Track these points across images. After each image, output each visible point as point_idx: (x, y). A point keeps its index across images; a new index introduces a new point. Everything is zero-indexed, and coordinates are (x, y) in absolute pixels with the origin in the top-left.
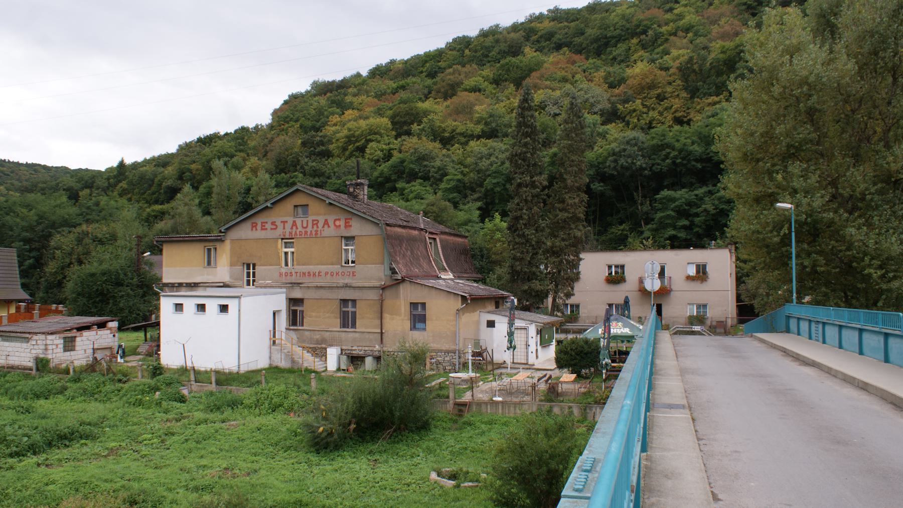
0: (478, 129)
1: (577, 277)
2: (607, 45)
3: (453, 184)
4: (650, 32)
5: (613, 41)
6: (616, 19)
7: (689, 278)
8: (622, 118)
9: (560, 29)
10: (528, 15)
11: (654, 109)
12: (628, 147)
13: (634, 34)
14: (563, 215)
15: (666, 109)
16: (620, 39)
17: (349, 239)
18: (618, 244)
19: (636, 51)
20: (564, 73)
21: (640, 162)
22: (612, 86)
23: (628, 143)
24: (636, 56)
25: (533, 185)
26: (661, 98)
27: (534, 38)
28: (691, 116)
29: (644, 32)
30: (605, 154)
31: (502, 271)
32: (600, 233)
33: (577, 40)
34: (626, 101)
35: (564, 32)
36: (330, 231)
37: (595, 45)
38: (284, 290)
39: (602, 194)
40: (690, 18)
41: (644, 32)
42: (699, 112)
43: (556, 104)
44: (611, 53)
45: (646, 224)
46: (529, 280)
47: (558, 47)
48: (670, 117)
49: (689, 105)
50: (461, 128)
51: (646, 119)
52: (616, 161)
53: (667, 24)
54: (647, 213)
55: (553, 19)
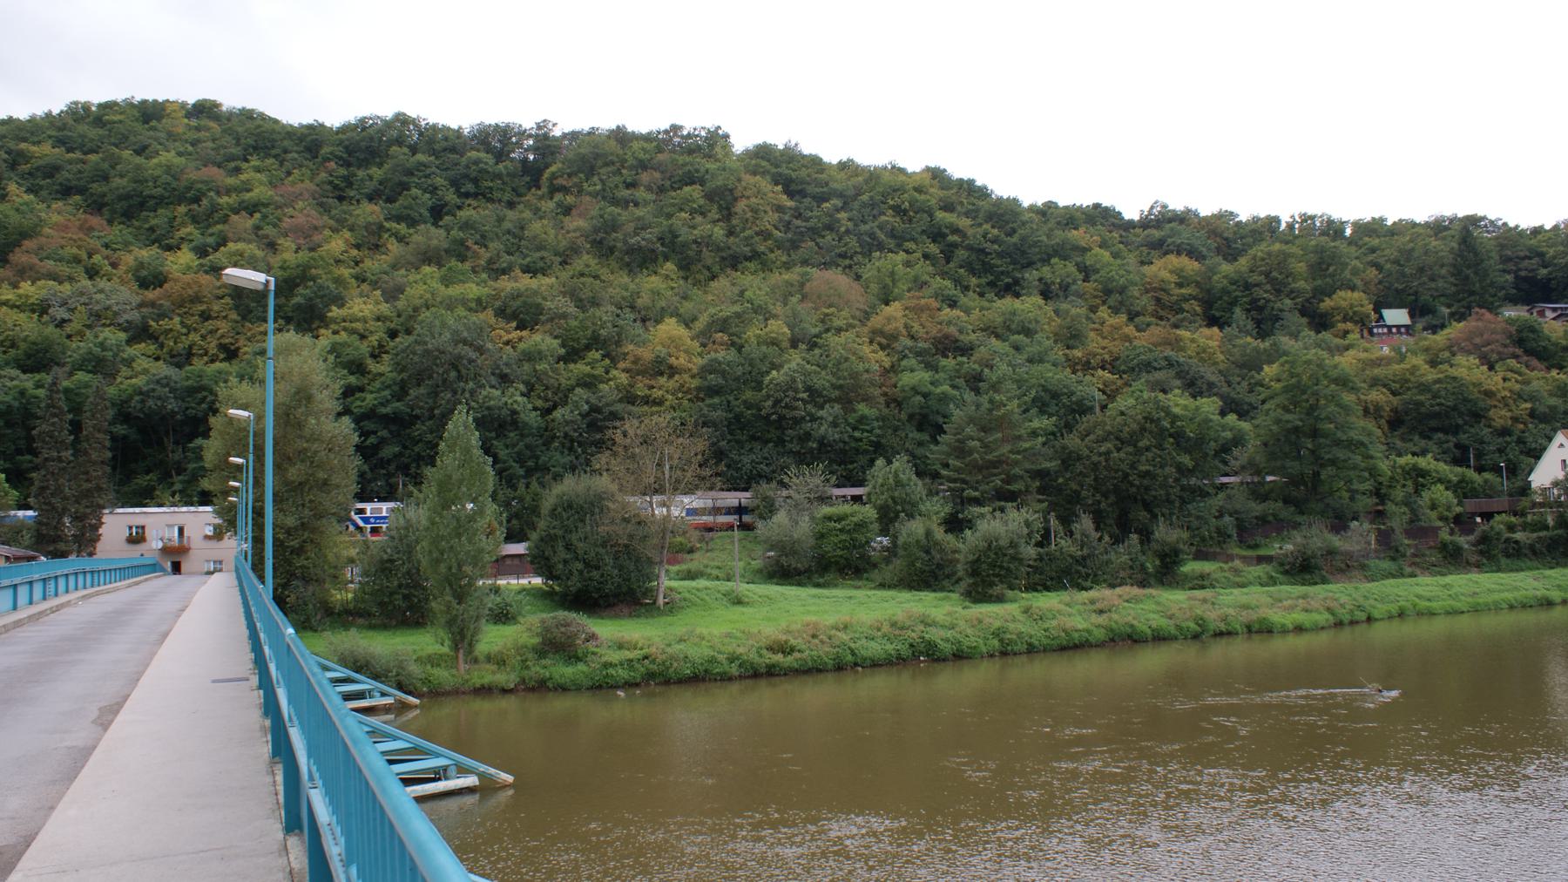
1: (98, 538)
2: (142, 205)
4: (205, 202)
5: (152, 202)
6: (158, 172)
7: (207, 537)
9: (70, 162)
11: (195, 330)
12: (158, 387)
13: (181, 200)
14: (86, 486)
15: (211, 332)
16: (161, 201)
18: (143, 498)
19: (183, 224)
20: (75, 250)
21: (172, 405)
22: (144, 284)
23: (158, 382)
24: (183, 232)
25: (60, 459)
26: (206, 316)
27: (25, 168)
28: (240, 344)
29: (197, 200)
30: (130, 391)
31: (27, 538)
32: (121, 483)
33: (97, 188)
34: (162, 316)
35: (75, 168)
37: (124, 204)
39: (125, 437)
40: (260, 192)
41: (197, 200)
42: (249, 339)
43: (64, 304)
44: (146, 220)
45: (178, 474)
46: (54, 542)
47: (66, 192)
49: (240, 329)
51: (185, 343)
52: (143, 401)
53: (228, 192)
54: (179, 462)
55: (60, 142)
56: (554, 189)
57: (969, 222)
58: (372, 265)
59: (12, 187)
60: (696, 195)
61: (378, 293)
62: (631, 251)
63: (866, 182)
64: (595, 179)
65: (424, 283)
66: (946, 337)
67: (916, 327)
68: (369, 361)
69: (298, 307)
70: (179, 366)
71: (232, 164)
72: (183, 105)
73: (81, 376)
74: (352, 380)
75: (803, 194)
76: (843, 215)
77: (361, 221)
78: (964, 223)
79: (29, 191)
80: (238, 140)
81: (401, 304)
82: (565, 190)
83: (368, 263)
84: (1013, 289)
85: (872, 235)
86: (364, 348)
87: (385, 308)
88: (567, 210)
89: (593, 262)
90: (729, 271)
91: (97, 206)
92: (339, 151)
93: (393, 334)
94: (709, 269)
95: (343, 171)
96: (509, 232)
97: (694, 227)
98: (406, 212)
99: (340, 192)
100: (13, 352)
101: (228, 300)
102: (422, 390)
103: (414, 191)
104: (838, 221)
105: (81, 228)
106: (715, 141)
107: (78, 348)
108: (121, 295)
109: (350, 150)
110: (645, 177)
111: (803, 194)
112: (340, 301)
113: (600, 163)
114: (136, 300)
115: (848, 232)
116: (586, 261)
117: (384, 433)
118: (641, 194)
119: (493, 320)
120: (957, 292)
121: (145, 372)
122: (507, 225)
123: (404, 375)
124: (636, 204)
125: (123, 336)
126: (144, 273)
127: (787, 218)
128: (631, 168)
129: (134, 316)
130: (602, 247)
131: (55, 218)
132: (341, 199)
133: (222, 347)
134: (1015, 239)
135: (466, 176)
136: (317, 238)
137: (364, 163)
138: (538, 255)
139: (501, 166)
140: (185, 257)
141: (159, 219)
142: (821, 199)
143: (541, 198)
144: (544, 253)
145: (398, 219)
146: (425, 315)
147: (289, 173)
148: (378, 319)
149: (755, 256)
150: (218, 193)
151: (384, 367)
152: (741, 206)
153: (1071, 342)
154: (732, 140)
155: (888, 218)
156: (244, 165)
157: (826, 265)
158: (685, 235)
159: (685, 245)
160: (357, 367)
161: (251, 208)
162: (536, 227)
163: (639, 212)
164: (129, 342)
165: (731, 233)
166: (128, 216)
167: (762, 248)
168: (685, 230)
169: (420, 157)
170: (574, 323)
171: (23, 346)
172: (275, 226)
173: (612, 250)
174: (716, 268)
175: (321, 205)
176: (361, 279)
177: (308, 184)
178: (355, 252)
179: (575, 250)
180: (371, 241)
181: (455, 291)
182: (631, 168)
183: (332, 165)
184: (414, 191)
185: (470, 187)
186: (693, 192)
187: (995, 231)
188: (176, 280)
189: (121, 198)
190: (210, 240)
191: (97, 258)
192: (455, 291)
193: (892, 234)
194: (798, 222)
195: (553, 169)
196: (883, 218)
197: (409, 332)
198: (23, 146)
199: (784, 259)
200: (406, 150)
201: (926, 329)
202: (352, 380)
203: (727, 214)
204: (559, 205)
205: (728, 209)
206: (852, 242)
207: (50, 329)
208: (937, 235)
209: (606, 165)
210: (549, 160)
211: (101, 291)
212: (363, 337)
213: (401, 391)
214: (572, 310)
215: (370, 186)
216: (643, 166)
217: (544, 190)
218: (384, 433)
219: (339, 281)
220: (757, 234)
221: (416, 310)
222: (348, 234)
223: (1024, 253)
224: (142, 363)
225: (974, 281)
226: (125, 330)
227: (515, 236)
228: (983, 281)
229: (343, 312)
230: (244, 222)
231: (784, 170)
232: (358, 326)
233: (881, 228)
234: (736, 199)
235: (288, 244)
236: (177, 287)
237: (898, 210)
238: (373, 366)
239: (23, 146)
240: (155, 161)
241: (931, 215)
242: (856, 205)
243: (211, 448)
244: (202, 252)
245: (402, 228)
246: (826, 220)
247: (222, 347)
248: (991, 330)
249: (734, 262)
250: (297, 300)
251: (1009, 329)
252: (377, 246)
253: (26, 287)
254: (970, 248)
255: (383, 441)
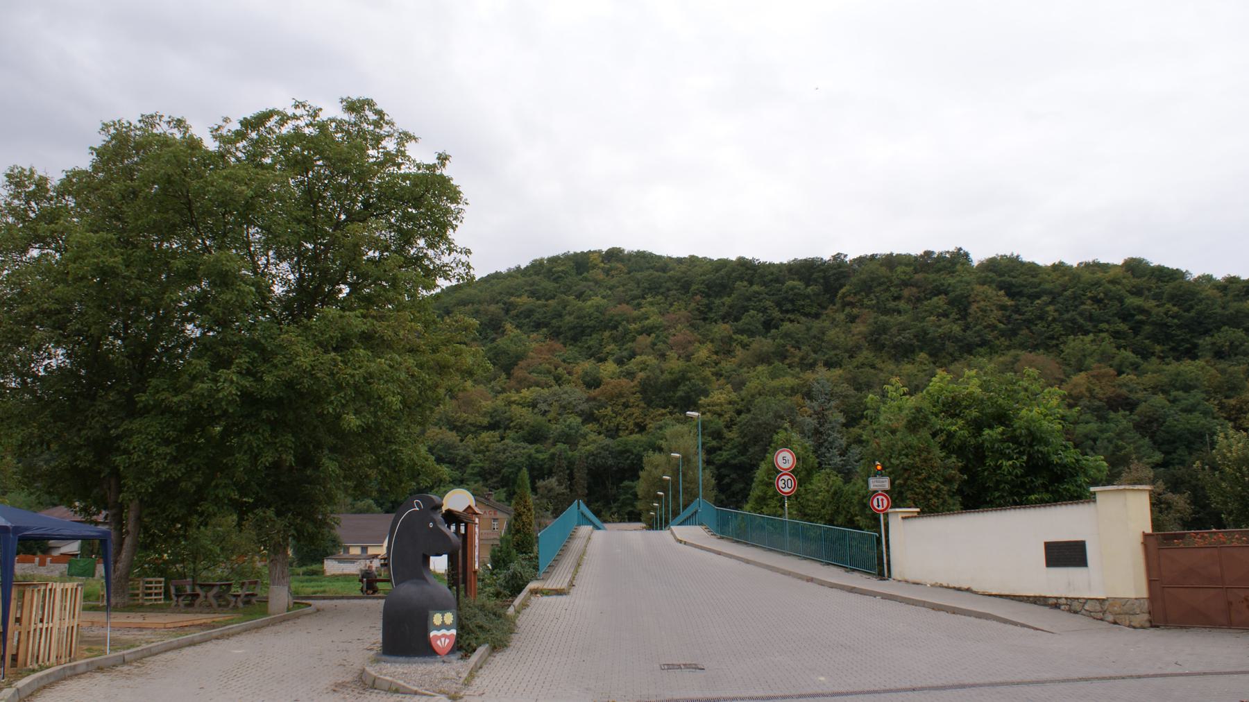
0: (486, 421)
2: (583, 333)
3: (476, 470)
4: (620, 328)
5: (588, 331)
6: (592, 310)
8: (596, 420)
10: (460, 189)
13: (606, 328)
16: (594, 329)
17: (495, 520)
19: (608, 343)
21: (610, 462)
26: (626, 406)
27: (514, 312)
36: (487, 516)
38: (1148, 487)
40: (654, 319)
41: (615, 327)
44: (586, 342)
47: (538, 326)
48: (632, 422)
50: (471, 419)
53: (635, 320)
55: (532, 294)
56: (845, 305)
57: (1154, 303)
58: (727, 365)
59: (508, 326)
60: (941, 303)
61: (729, 386)
62: (895, 346)
63: (1070, 280)
64: (872, 296)
65: (759, 377)
66: (1119, 396)
67: (1097, 389)
68: (725, 430)
69: (681, 398)
70: (612, 437)
71: (635, 300)
72: (600, 252)
73: (560, 445)
74: (714, 443)
75: (1021, 294)
76: (1051, 308)
77: (718, 336)
78: (1150, 304)
79: (517, 327)
80: (638, 283)
81: (743, 393)
82: (852, 305)
83: (723, 364)
84: (1192, 353)
85: (1073, 321)
86: (721, 423)
87: (734, 396)
88: (853, 319)
89: (871, 355)
90: (965, 355)
91: (556, 334)
92: (702, 287)
93: (739, 413)
94: (951, 355)
95: (705, 301)
96: (815, 337)
97: (940, 326)
98: (747, 327)
99: (705, 315)
100: (521, 432)
101: (638, 395)
102: (757, 448)
103: (752, 312)
104: (1047, 312)
105: (549, 351)
106: (959, 258)
107: (556, 428)
108: (576, 393)
109: (709, 287)
110: (906, 292)
111: (1021, 294)
112: (706, 393)
113: (875, 284)
114: (585, 396)
115: (1054, 320)
116: (866, 355)
117: (734, 476)
118: (902, 305)
119: (801, 401)
120: (1138, 360)
121: (594, 441)
122: (814, 332)
123: (746, 439)
124: (899, 312)
125: (579, 420)
126: (588, 379)
127: (1008, 313)
128: (896, 286)
129: (585, 407)
130: (876, 341)
131: (534, 345)
132: (705, 319)
133: (637, 425)
134: (1192, 313)
135: (786, 299)
136: (691, 349)
137: (718, 295)
138: (833, 353)
139: (809, 290)
140: (610, 367)
141: (592, 341)
142: (1038, 296)
143: (836, 311)
144: (838, 352)
145: (741, 332)
146: (759, 400)
147: (671, 305)
148: (730, 403)
149: (984, 343)
150: (628, 322)
151: (733, 435)
152: (973, 308)
153: (1228, 393)
154: (971, 256)
155: (1088, 306)
156: (644, 301)
157: (1035, 348)
158: (933, 332)
159: (933, 340)
160: (717, 435)
161: (648, 331)
162: (832, 334)
163: (901, 319)
164: (583, 423)
165: (966, 328)
166: (575, 339)
167: (990, 337)
168: (932, 329)
169: (755, 288)
170: (853, 400)
171: (527, 428)
172: (664, 342)
173: (883, 346)
174: (957, 354)
175: (692, 325)
176: (718, 375)
177: (683, 312)
178: (715, 357)
179: (859, 348)
180: (725, 349)
181: (776, 383)
182: (896, 286)
183: (698, 297)
184: (752, 312)
185: (789, 306)
186: (939, 301)
187: (1175, 309)
188: (608, 384)
189: (570, 329)
190: (625, 353)
191: (560, 370)
192: (776, 383)
193: (1090, 318)
194: (1016, 316)
195: (843, 290)
196: (1083, 307)
197: (749, 411)
198: (512, 299)
199: (1007, 343)
200: (745, 283)
201: (1104, 391)
202: (714, 443)
203: (964, 314)
204: (849, 315)
205: (965, 310)
206: (1058, 327)
207: (540, 418)
208: (1126, 316)
209: (880, 284)
210: (842, 281)
211: (566, 392)
212: (720, 415)
213: (743, 449)
214: (852, 392)
215: (724, 310)
216: (905, 284)
217: (838, 305)
218: (734, 476)
219: (705, 379)
220: (985, 327)
221: (753, 396)
222: (710, 345)
223: (1200, 323)
224: (593, 436)
225: (1158, 348)
226: (580, 416)
227: (819, 339)
228: (1166, 348)
229: (708, 400)
230: (644, 340)
231: (1007, 278)
232: (717, 408)
233: (1081, 314)
234: (970, 303)
235: (672, 354)
236: (609, 387)
237: (1096, 300)
238: (728, 435)
239: (512, 299)
240: (589, 303)
241: (1121, 300)
242: (1061, 299)
243: (641, 487)
244: (620, 362)
245: (744, 338)
246: (1038, 313)
247: (637, 425)
248: (1156, 389)
249: (969, 349)
250: (680, 393)
251: (1174, 386)
252: (729, 352)
253: (525, 392)
254: (1154, 324)
255: (734, 480)
